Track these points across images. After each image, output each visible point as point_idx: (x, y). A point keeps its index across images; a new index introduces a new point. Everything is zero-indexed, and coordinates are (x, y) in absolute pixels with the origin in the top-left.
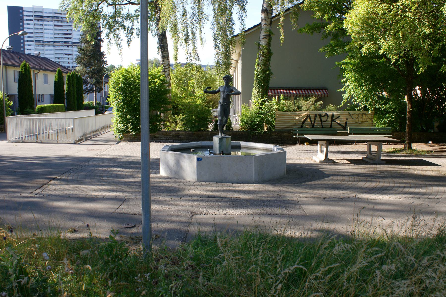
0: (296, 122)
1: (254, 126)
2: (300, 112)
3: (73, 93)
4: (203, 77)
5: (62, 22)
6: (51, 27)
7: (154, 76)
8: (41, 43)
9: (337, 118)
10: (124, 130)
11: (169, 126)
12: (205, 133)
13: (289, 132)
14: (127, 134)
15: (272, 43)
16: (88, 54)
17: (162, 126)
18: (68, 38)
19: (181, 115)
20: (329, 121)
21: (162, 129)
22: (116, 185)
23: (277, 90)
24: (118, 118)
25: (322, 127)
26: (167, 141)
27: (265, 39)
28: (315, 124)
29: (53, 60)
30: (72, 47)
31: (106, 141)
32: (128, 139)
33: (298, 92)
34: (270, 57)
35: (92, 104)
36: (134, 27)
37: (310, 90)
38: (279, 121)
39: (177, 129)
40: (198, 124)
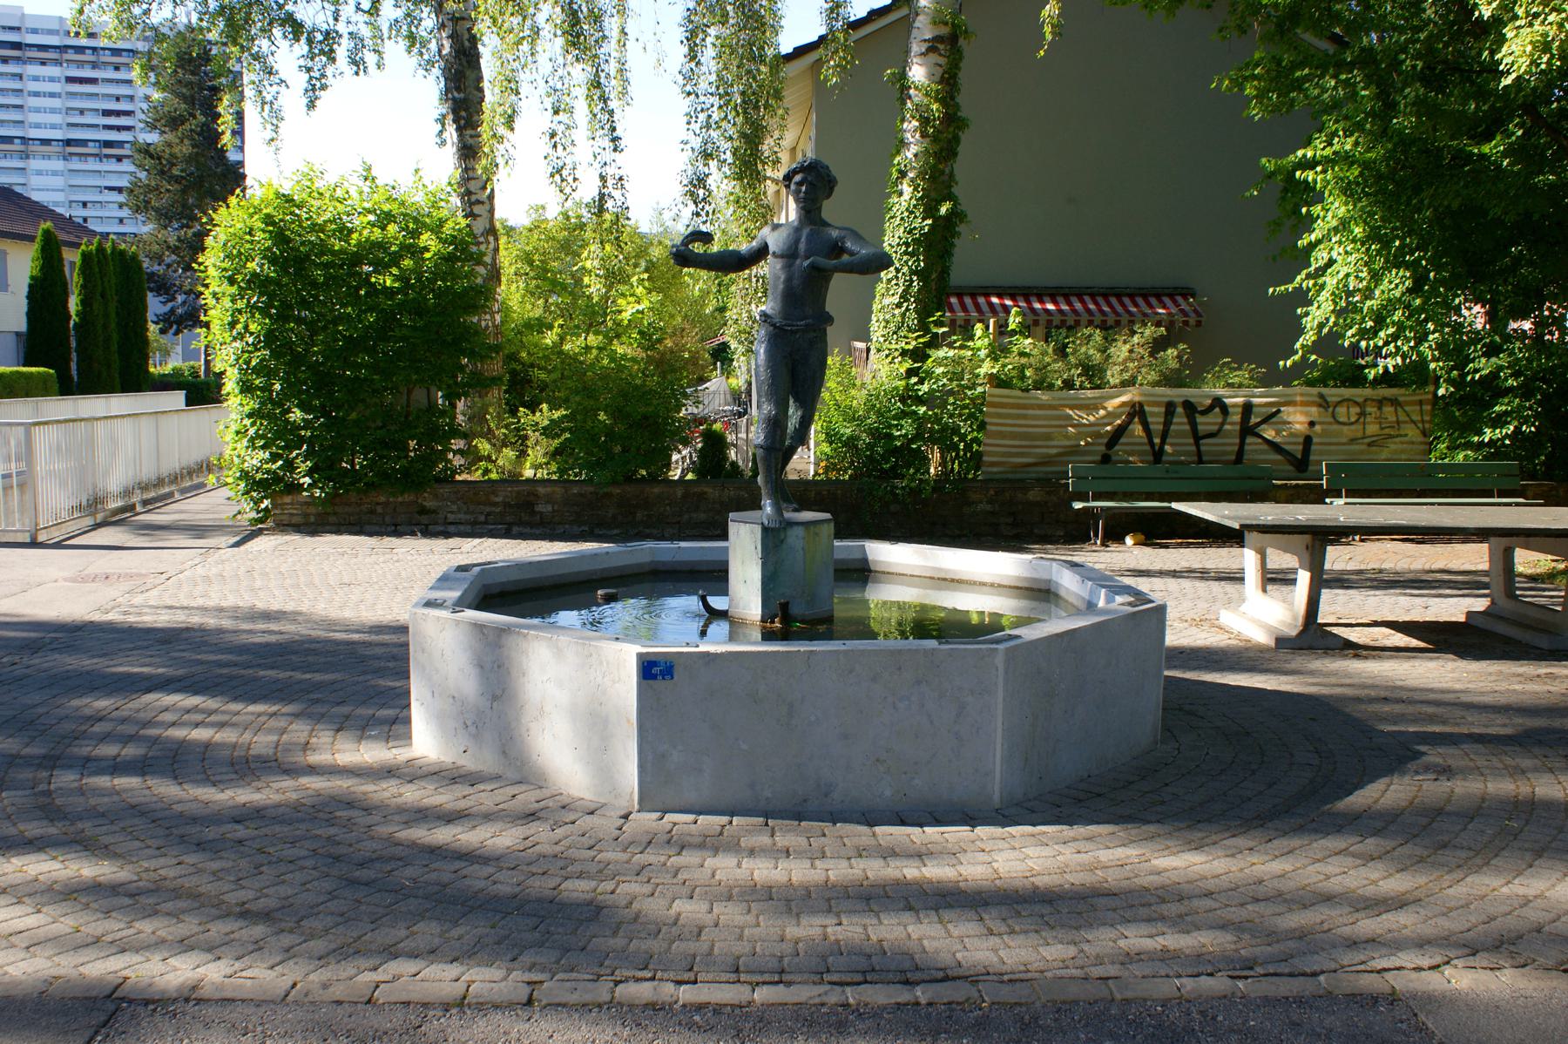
0: (1079, 436)
1: (885, 458)
2: (1097, 393)
3: (105, 327)
4: (637, 256)
5: (95, 65)
6: (56, 87)
7: (416, 220)
8: (17, 146)
9: (1264, 421)
10: (276, 478)
11: (489, 459)
12: (656, 490)
13: (1052, 483)
14: (288, 499)
15: (963, 77)
16: (176, 172)
17: (458, 461)
18: (119, 128)
19: (545, 406)
20: (1229, 434)
21: (454, 472)
23: (987, 296)
24: (247, 422)
25: (1200, 461)
26: (478, 529)
27: (933, 58)
28: (1168, 448)
29: (60, 210)
31: (199, 530)
32: (295, 520)
33: (1065, 307)
34: (956, 139)
35: (195, 374)
36: (342, 27)
37: (1119, 297)
38: (1003, 435)
39: (528, 473)
40: (625, 450)
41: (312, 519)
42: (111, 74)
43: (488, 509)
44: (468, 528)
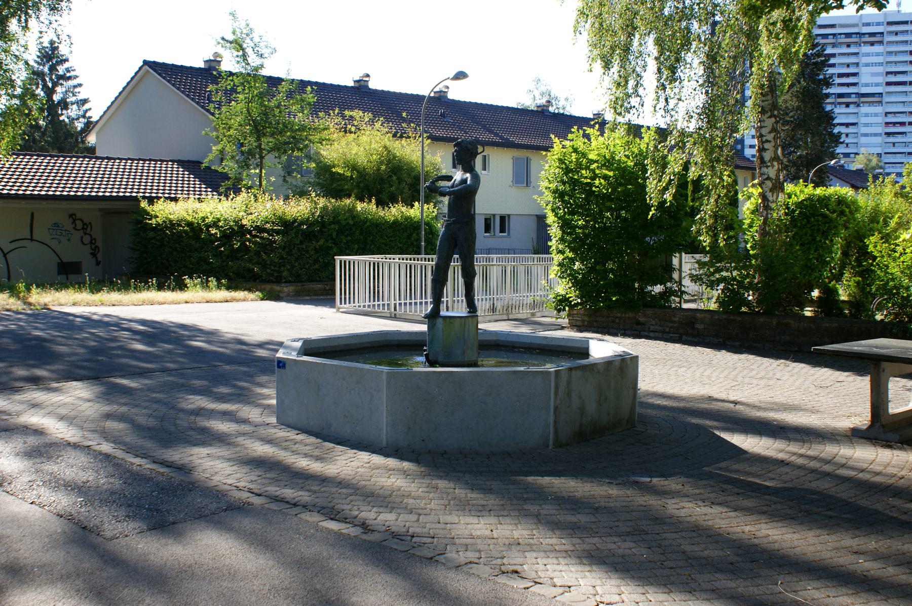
18: (848, 85)
22: (731, 478)
30: (858, 106)
32: (578, 323)
41: (586, 323)
42: (845, 50)
43: (671, 325)
44: (660, 335)
